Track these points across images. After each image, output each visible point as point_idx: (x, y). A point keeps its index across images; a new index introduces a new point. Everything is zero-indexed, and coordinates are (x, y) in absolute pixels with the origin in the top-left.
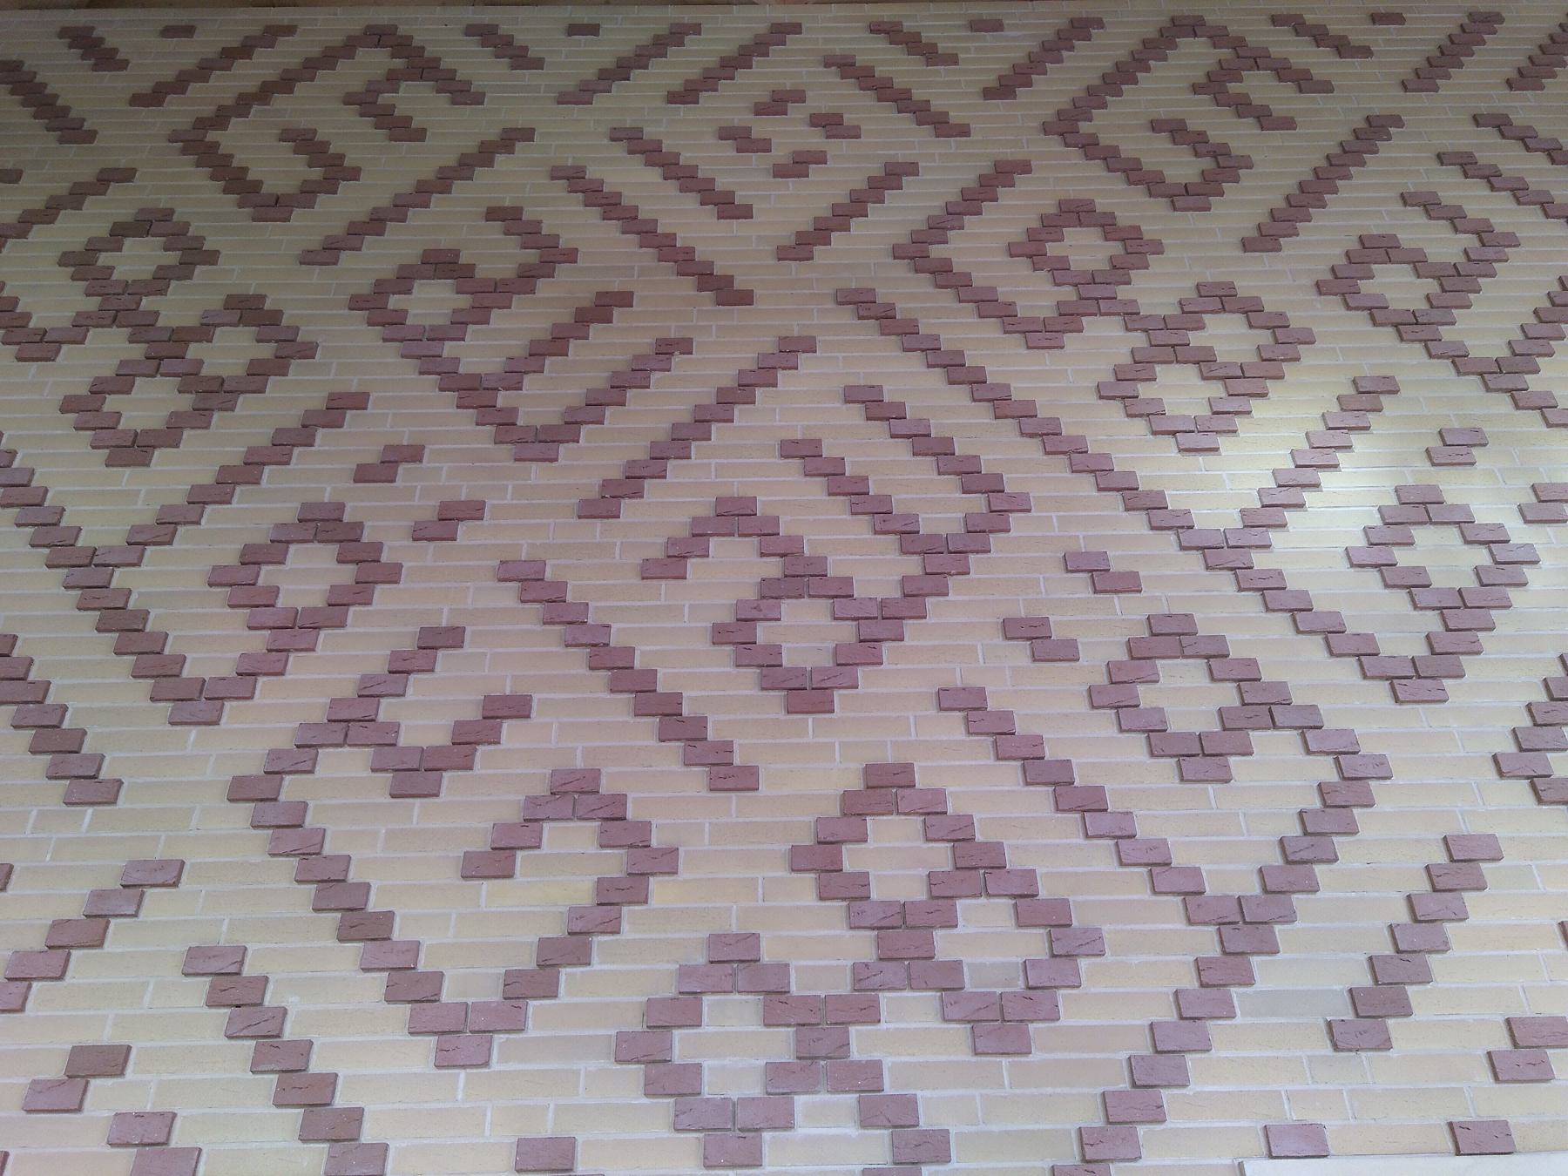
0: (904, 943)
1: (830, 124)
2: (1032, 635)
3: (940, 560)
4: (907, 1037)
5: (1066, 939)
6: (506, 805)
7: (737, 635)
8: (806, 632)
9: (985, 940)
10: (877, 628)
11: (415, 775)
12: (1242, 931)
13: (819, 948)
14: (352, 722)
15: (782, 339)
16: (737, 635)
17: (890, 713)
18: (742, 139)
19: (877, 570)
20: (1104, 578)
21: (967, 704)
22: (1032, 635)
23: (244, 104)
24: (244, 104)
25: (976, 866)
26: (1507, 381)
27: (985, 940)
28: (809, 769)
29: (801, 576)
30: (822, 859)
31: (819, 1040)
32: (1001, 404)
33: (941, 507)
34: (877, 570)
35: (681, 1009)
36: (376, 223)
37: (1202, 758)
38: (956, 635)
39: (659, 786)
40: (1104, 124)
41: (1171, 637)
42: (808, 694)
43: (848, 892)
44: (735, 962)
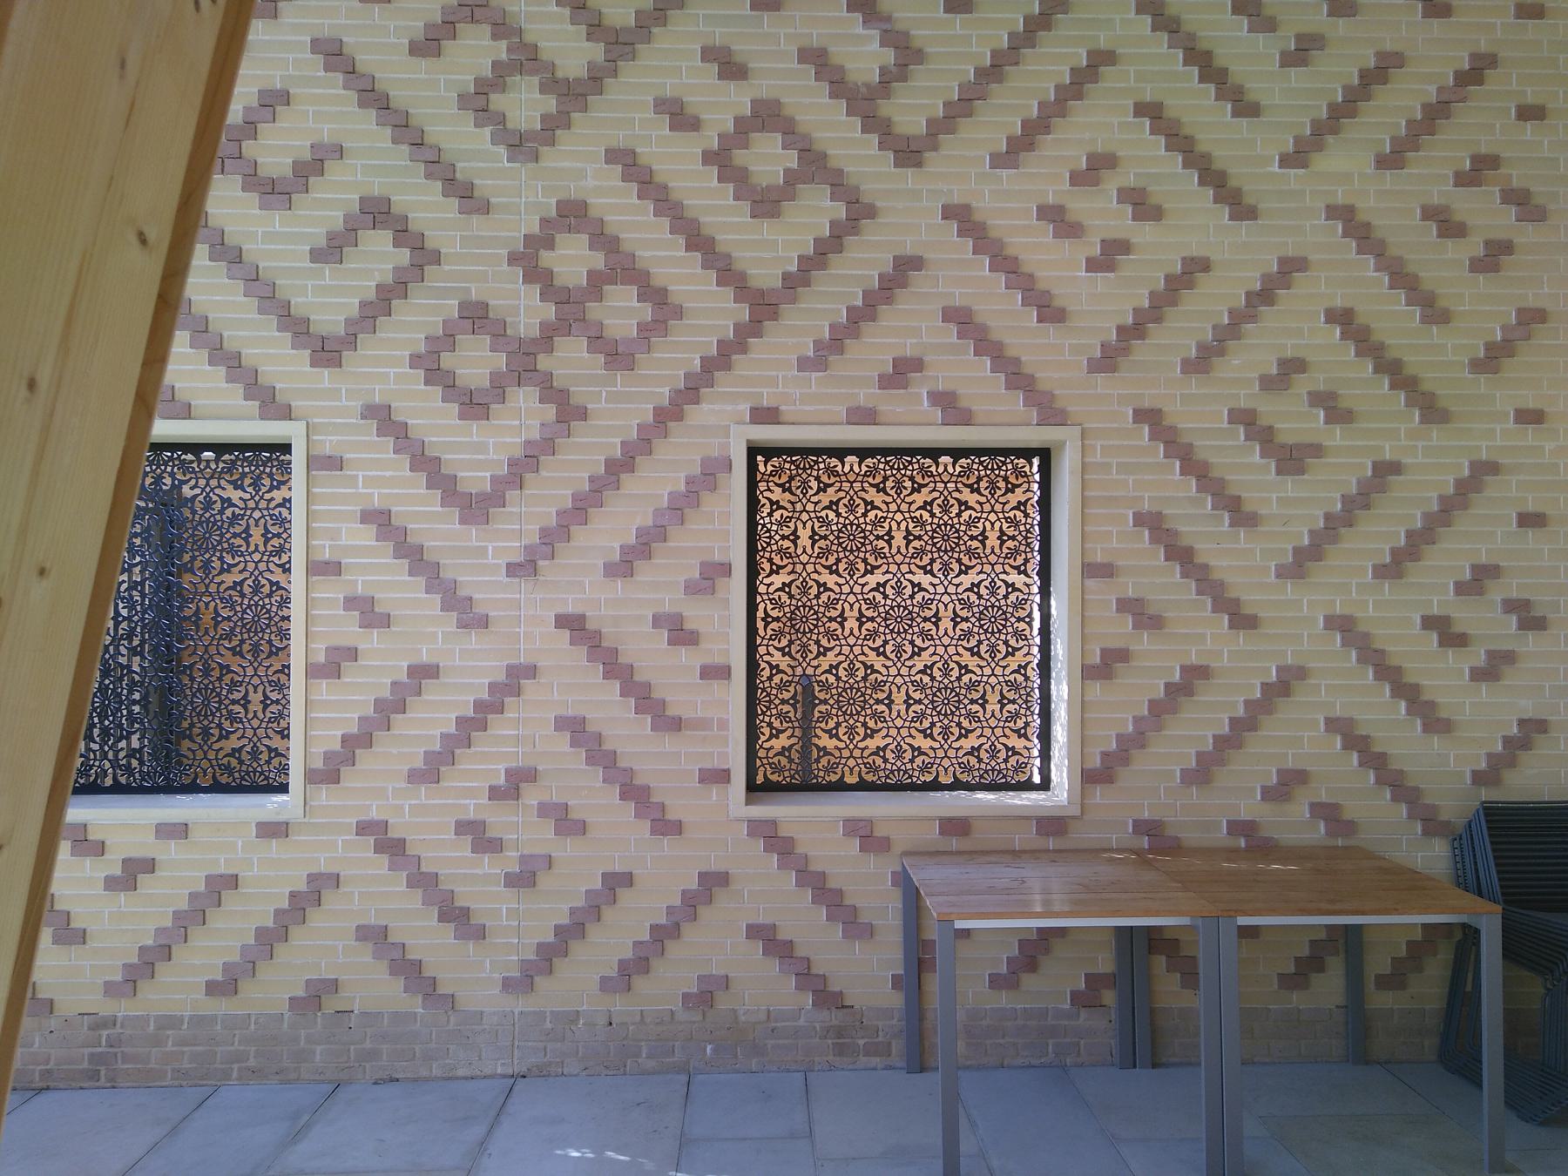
2: (680, 117)
4: (571, 360)
6: (335, 219)
7: (479, 101)
8: (525, 104)
9: (621, 311)
12: (763, 309)
13: (528, 312)
15: (919, 164)
17: (579, 166)
20: (731, 68)
21: (626, 161)
22: (680, 117)
25: (621, 268)
27: (621, 311)
28: (523, 197)
30: (529, 261)
31: (524, 362)
34: (573, 53)
35: (446, 340)
37: (767, 204)
38: (625, 112)
39: (424, 204)
43: (538, 275)
44: (476, 316)
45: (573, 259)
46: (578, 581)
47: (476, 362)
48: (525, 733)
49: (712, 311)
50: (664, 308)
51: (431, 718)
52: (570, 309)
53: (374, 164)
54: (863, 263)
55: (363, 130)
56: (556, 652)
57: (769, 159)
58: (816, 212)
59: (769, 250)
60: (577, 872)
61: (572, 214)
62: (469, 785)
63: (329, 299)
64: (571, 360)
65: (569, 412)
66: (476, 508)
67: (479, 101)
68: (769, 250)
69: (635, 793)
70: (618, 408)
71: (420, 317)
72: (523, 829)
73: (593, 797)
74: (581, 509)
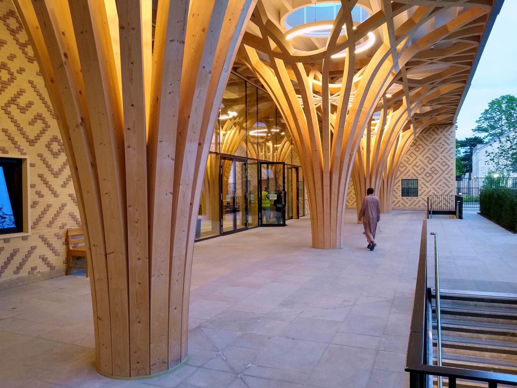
0: (433, 172)
1: (432, 135)
3: (436, 158)
4: (433, 175)
5: (438, 172)
8: (430, 162)
10: (433, 161)
11: (23, 110)
13: (430, 172)
14: (415, 165)
16: (436, 174)
17: (433, 165)
18: (428, 136)
19: (433, 159)
23: (24, 134)
24: (24, 134)
25: (436, 170)
26: (22, 48)
27: (436, 172)
28: (430, 166)
29: (431, 159)
32: (425, 144)
33: (436, 156)
34: (433, 159)
36: (433, 183)
38: (436, 162)
40: (56, 168)
41: (444, 161)
44: (428, 173)
45: (433, 170)
46: (433, 185)
47: (428, 175)
48: (441, 150)
49: (441, 172)
50: (438, 172)
51: (446, 151)
52: (433, 172)
54: (450, 169)
55: (421, 163)
56: (432, 189)
57: (444, 164)
58: (431, 177)
59: (444, 169)
60: (438, 144)
61: (433, 167)
62: (444, 147)
63: (420, 172)
64: (433, 175)
65: (433, 177)
66: (428, 182)
68: (444, 169)
69: (435, 147)
70: (435, 177)
72: (441, 146)
73: (437, 147)
74: (433, 183)
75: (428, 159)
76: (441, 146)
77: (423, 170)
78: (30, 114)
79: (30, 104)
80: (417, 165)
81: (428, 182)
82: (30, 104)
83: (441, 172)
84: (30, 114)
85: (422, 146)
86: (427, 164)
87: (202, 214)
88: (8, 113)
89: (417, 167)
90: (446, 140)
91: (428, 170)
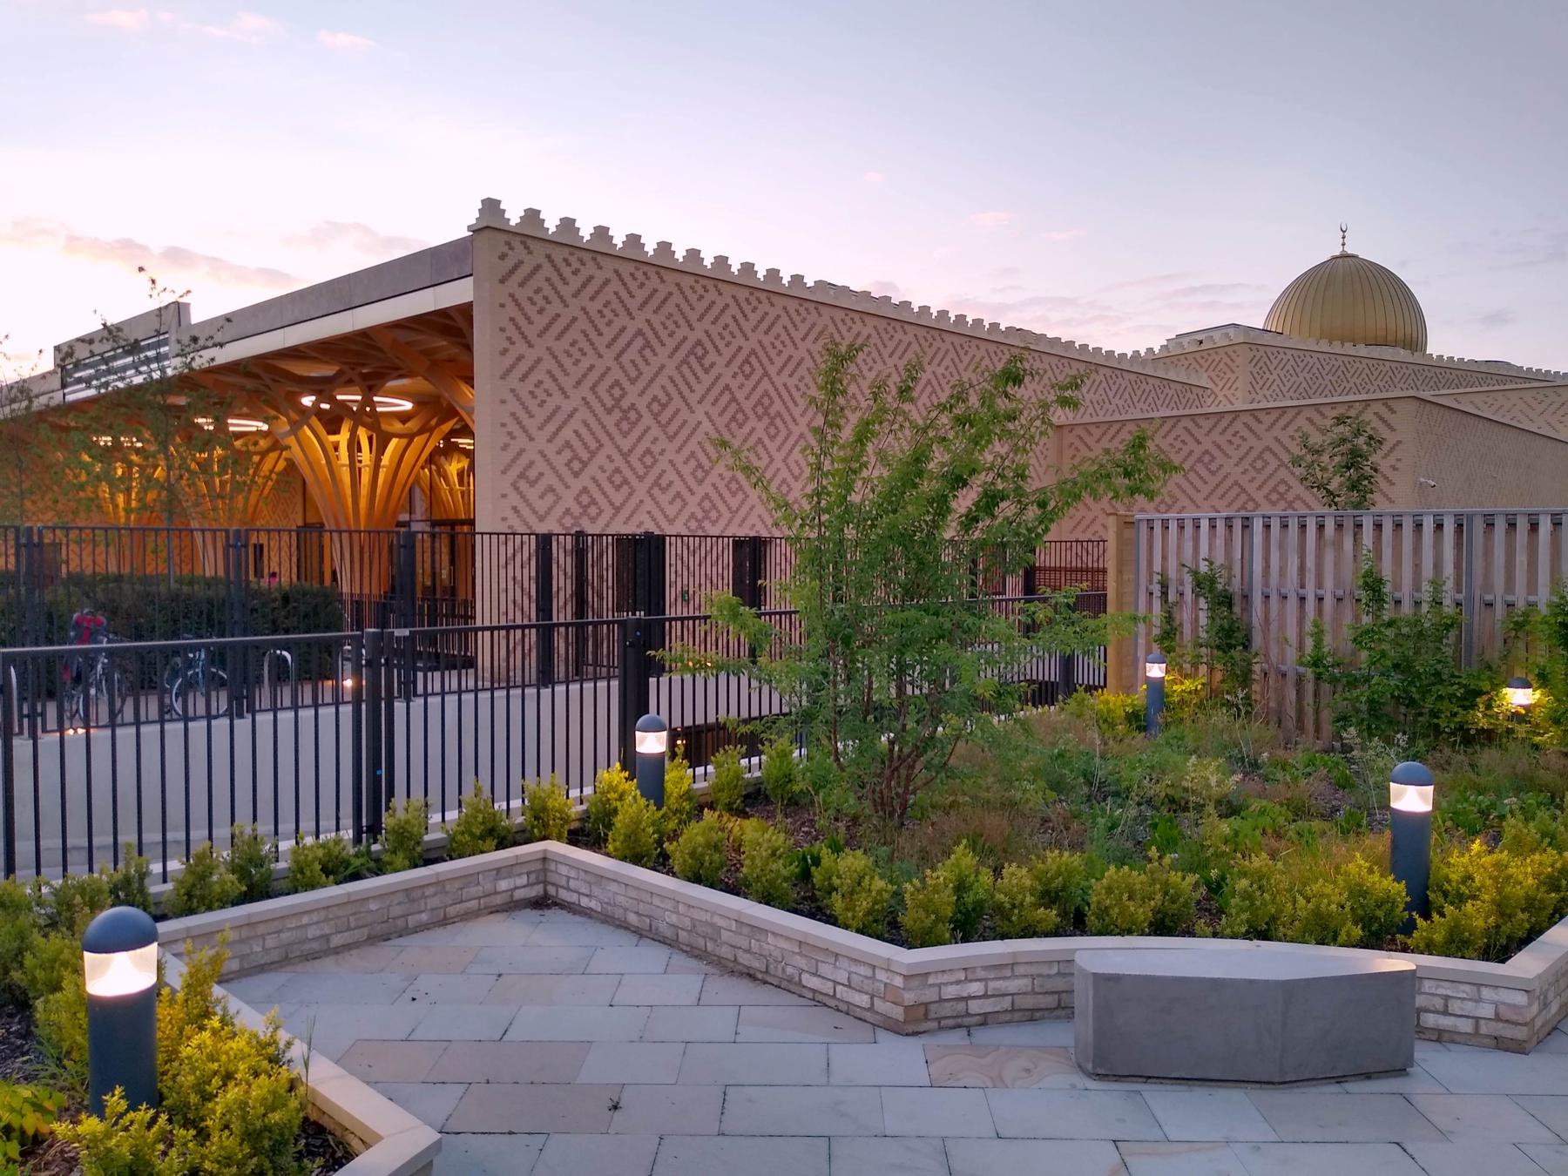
3: (1244, 491)
11: (532, 483)
27: (1282, 488)
39: (685, 493)
42: (747, 418)
50: (625, 435)
53: (648, 372)
58: (1267, 456)
65: (609, 411)
66: (593, 388)
67: (568, 464)
71: (559, 510)
72: (1236, 441)
75: (567, 454)
76: (1178, 445)
77: (633, 374)
78: (541, 486)
79: (671, 484)
80: (647, 352)
81: (593, 388)
82: (671, 484)
83: (626, 444)
84: (541, 486)
85: (1275, 455)
86: (1216, 452)
87: (739, 544)
88: (517, 489)
89: (532, 483)
90: (1554, 407)
91: (632, 391)
